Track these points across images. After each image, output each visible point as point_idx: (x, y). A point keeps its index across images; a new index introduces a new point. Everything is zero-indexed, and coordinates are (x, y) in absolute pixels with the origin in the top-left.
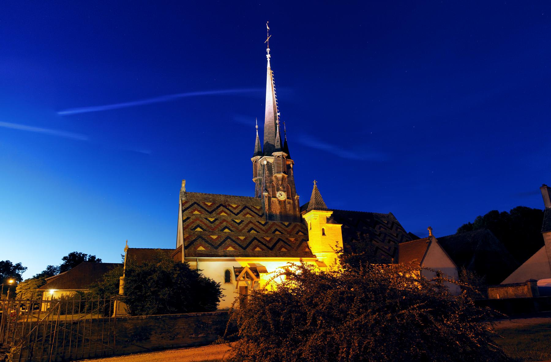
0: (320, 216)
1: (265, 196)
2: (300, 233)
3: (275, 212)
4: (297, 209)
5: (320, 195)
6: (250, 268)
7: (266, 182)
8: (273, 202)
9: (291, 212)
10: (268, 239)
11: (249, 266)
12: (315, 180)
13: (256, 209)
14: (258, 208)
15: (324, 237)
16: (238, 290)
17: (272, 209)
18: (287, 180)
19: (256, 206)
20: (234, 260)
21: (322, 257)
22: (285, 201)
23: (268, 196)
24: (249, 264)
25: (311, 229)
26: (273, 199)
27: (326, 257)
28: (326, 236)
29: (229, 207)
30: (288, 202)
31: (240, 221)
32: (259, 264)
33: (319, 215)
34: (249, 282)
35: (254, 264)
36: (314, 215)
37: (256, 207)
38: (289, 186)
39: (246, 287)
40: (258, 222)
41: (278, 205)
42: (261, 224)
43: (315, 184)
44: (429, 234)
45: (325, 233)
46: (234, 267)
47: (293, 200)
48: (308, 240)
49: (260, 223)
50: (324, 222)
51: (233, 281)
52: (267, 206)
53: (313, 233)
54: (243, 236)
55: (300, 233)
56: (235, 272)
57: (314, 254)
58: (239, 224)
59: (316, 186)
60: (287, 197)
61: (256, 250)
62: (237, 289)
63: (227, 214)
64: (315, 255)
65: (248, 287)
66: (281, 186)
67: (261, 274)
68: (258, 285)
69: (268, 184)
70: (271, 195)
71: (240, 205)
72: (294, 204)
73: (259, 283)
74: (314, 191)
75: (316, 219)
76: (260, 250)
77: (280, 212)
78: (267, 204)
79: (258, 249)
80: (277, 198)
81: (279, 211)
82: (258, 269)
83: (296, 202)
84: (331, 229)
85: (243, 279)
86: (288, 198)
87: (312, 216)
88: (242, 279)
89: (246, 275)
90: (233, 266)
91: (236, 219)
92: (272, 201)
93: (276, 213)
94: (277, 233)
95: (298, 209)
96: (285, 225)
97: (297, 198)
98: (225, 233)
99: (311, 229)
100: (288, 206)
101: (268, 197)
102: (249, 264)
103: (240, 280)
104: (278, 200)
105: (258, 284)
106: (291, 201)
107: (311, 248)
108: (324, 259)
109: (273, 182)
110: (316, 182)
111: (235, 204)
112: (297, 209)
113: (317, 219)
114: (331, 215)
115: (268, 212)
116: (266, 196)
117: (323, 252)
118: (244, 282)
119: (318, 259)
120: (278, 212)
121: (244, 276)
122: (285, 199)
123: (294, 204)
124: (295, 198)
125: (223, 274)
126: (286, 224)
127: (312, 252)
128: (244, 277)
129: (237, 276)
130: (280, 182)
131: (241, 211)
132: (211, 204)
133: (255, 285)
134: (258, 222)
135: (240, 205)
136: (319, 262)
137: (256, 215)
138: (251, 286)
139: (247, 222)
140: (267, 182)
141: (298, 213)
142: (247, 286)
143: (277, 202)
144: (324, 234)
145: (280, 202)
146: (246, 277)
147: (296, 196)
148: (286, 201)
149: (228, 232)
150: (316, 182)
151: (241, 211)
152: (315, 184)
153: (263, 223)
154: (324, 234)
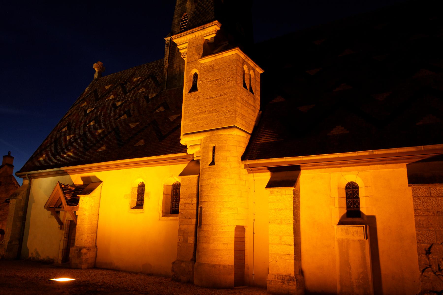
32: (95, 177)
79: (338, 130)
102: (83, 178)
114: (218, 32)
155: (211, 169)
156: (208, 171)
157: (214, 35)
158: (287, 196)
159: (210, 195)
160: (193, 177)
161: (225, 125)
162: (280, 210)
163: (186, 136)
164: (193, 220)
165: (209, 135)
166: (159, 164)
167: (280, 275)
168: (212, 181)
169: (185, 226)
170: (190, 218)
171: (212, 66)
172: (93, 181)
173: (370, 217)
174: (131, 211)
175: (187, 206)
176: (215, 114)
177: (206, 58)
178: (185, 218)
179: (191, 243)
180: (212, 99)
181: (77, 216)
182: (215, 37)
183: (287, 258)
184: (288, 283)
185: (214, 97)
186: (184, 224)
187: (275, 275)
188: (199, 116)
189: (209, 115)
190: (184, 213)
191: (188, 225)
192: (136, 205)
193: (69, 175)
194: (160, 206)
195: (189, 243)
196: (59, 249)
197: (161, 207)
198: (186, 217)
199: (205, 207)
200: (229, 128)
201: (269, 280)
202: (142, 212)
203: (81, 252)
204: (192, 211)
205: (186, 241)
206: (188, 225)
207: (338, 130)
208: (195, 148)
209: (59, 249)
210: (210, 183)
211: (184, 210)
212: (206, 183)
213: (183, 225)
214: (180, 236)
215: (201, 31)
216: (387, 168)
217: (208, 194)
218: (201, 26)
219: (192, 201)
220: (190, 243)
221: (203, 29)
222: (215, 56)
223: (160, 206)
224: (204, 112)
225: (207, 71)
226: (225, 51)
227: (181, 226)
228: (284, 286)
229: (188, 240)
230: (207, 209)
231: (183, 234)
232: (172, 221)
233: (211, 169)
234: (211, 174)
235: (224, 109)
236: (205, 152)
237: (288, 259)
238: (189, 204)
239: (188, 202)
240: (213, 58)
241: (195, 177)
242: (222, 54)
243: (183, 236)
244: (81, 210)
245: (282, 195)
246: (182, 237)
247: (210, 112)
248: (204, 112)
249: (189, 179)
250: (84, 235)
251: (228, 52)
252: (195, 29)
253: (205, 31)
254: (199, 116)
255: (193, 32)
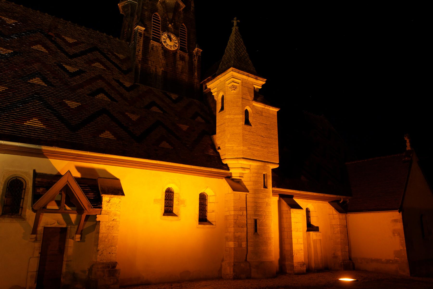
0: (244, 84)
1: (138, 34)
2: (199, 119)
3: (154, 69)
4: (196, 74)
5: (244, 46)
6: (81, 178)
7: (143, 8)
8: (152, 49)
9: (185, 77)
10: (134, 117)
11: (78, 175)
12: (235, 18)
13: (117, 57)
14: (121, 56)
15: (248, 127)
16: (36, 238)
17: (150, 63)
18: (182, 16)
19: (119, 53)
20: (40, 154)
21: (241, 171)
22: (175, 52)
23: (144, 34)
24: (79, 169)
25: (222, 109)
26: (153, 43)
27: (247, 171)
28: (251, 125)
29: (57, 39)
30: (180, 56)
31: (77, 69)
32: (105, 171)
33: (242, 82)
34: (73, 217)
35: (92, 170)
36: (232, 79)
37: (118, 55)
38: (185, 29)
39: (63, 231)
40: (118, 81)
41: (161, 56)
42: (124, 87)
43: (235, 24)
44: (407, 146)
45: (250, 120)
46: (37, 171)
47: (191, 55)
48: (215, 133)
49: (121, 84)
50: (249, 98)
51: (27, 210)
52: (140, 53)
53: (227, 117)
54: (78, 102)
55: (199, 119)
56: (35, 186)
57: (225, 162)
58: (73, 75)
59: (237, 28)
60: (180, 47)
61: (103, 136)
62: (34, 236)
63: (47, 50)
64: (226, 165)
65: (69, 229)
66: (171, 24)
67: (105, 198)
68: (96, 224)
69: (146, 13)
70: (151, 34)
71: (83, 43)
72: (191, 63)
73: (98, 220)
74: (232, 37)
75: (234, 88)
76: (111, 137)
77: (164, 72)
78: (141, 50)
79: (107, 135)
80: (161, 43)
81: (162, 69)
82: (100, 183)
83: (195, 61)
84: (260, 113)
85: (56, 207)
86: (181, 49)
87: (227, 82)
88: (53, 206)
89: (64, 195)
90: (34, 171)
91: (67, 64)
92: (150, 47)
93: (156, 71)
94: (154, 109)
95: (197, 73)
96: (171, 99)
97: (197, 53)
98: (33, 85)
99: (222, 109)
100: (180, 64)
101: (145, 37)
102: (79, 169)
103: (44, 209)
104: (162, 48)
105: (95, 223)
106: (186, 56)
107: (219, 148)
108: (243, 174)
109: (157, 11)
110: (239, 21)
111: (72, 37)
112: (196, 74)
113: (237, 90)
114: (263, 86)
115: (140, 66)
116: (140, 34)
117: (243, 158)
118: (59, 216)
119: (231, 173)
120: (160, 70)
121: (58, 198)
122: (176, 48)
123: (191, 63)
124: (194, 52)
125: (161, 196)
126: (174, 96)
127: (222, 158)
128: (58, 203)
129: (36, 197)
130: (171, 16)
131: (83, 53)
132: (79, 107)
133: (89, 224)
134: (118, 81)
135: (83, 43)
136: (233, 180)
137: (115, 68)
138: (76, 227)
139: (93, 76)
140: (145, 8)
141: (196, 81)
142: (65, 226)
143: (161, 51)
144: (247, 122)
145: (166, 51)
146: (64, 200)
147: (196, 49)
148: (177, 52)
149: (40, 85)
150: (239, 21)
151: (83, 53)
152: (235, 24)
153: (128, 84)
154: (247, 122)
155: (265, 191)
156: (263, 192)
157: (260, 88)
158: (299, 214)
159: (266, 210)
160: (243, 194)
161: (273, 161)
162: (297, 222)
163: (244, 160)
164: (244, 228)
165: (263, 165)
166: (212, 176)
167: (299, 262)
168: (267, 200)
169: (239, 234)
170: (242, 227)
171: (262, 112)
172: (101, 176)
173: (54, 212)
174: (163, 218)
175: (239, 217)
176: (266, 150)
177: (259, 103)
178: (239, 227)
179: (244, 247)
180: (263, 138)
181: (99, 221)
182: (259, 89)
183: (301, 252)
184: (303, 266)
185: (264, 136)
186: (239, 232)
187: (297, 263)
188: (255, 147)
189: (261, 149)
190: (237, 222)
191: (241, 232)
192: (311, 223)
193: (47, 159)
194: (197, 214)
195: (243, 247)
196: (28, 272)
197: (197, 215)
198: (239, 226)
199: (262, 219)
200: (275, 164)
201: (295, 267)
202: (177, 219)
203: (116, 269)
204: (243, 221)
205: (240, 246)
206: (241, 232)
207: (107, 135)
208: (246, 170)
209: (28, 272)
210: (266, 201)
211: (237, 220)
212: (262, 201)
213: (237, 233)
214: (236, 242)
215: (254, 79)
216: (322, 203)
217: (264, 210)
218: (256, 76)
219: (243, 213)
220: (244, 247)
221: (257, 79)
222: (265, 106)
223: (197, 214)
224: (258, 145)
225: (258, 113)
226: (263, 103)
227: (236, 233)
228: (301, 268)
229: (241, 245)
230: (264, 221)
231: (238, 240)
232: (205, 227)
233: (265, 191)
234: (266, 195)
235: (272, 149)
236: (259, 177)
237: (301, 253)
238: (241, 215)
239: (240, 214)
240: (264, 106)
241: (245, 194)
242: (270, 107)
243: (238, 241)
244: (107, 214)
245: (297, 214)
246: (237, 242)
247: (262, 147)
248: (258, 145)
249: (239, 195)
250: (114, 248)
251: (273, 108)
252: (251, 75)
253: (256, 81)
254: (255, 147)
255: (248, 76)
